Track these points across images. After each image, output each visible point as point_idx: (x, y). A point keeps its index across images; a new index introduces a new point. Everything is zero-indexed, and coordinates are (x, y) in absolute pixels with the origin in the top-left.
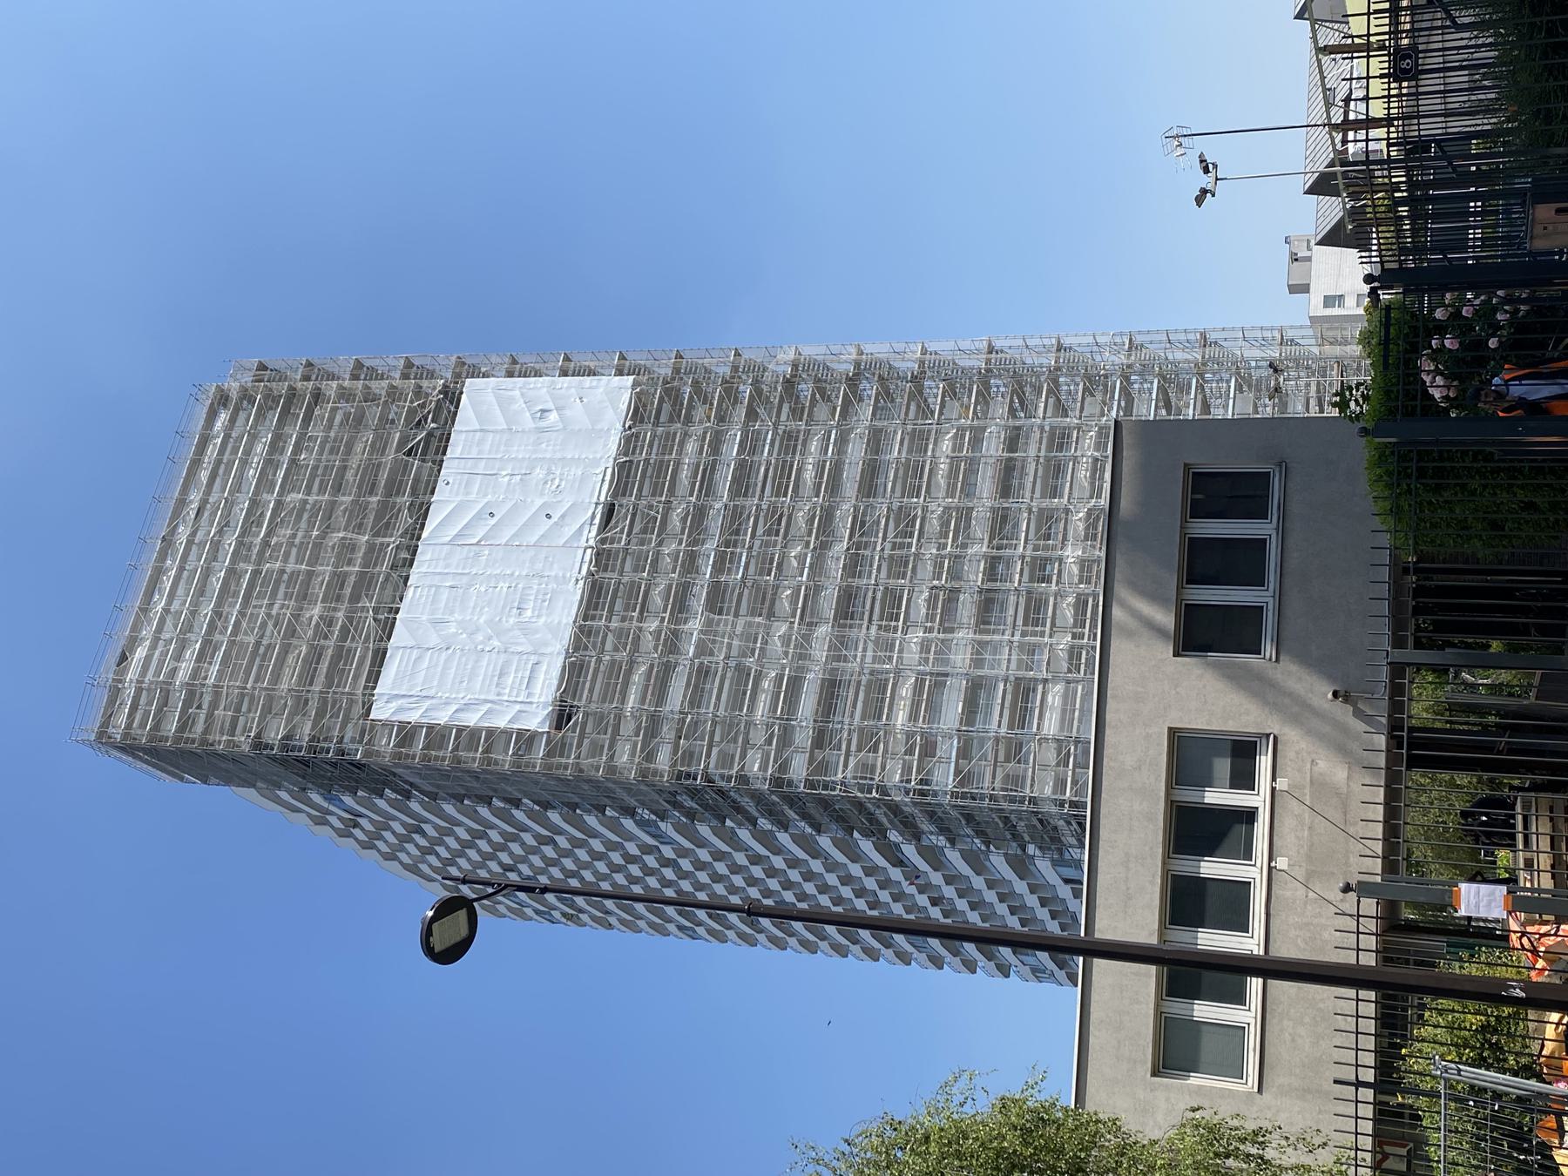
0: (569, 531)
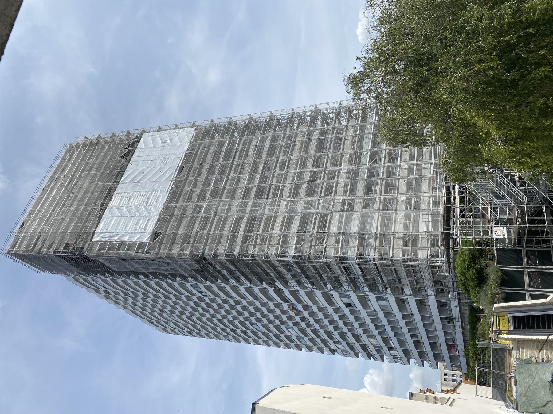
0: (167, 175)
